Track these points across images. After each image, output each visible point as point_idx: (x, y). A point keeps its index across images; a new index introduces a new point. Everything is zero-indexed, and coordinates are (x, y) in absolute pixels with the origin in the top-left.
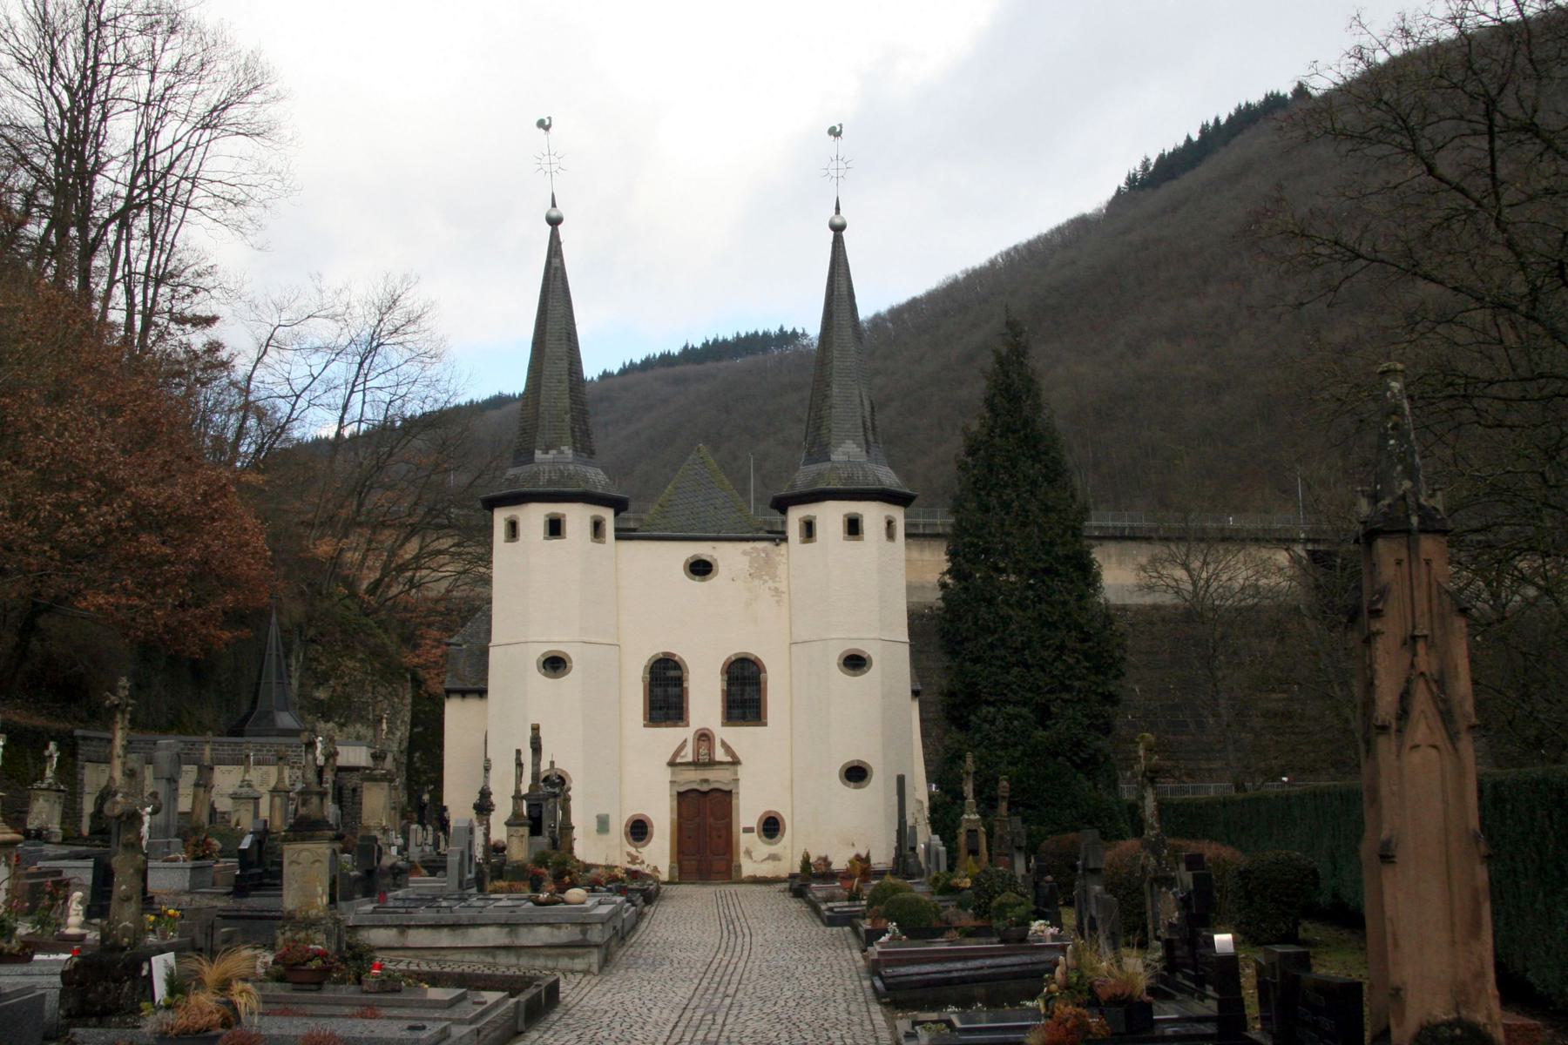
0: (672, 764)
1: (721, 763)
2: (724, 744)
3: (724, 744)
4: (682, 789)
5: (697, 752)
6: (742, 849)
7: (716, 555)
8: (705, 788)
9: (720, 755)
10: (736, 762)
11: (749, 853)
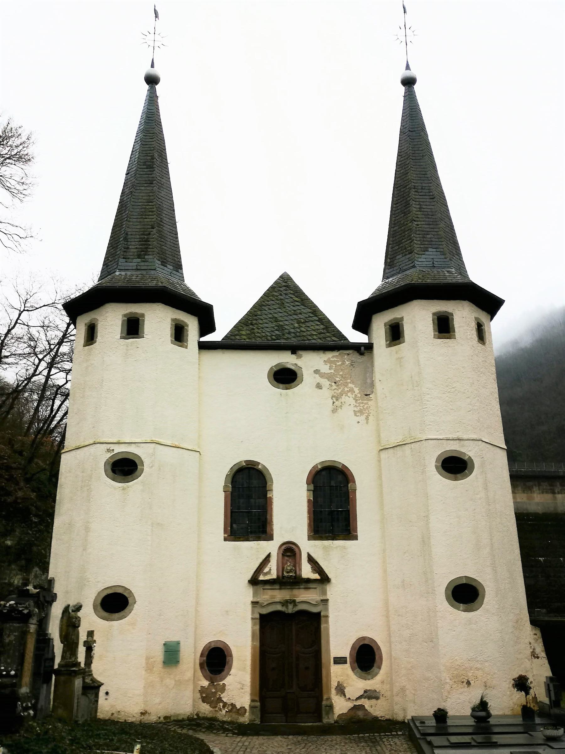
0: (254, 581)
1: (308, 581)
2: (311, 559)
3: (311, 559)
4: (265, 611)
5: (281, 567)
6: (334, 684)
7: (300, 362)
8: (290, 609)
9: (307, 571)
10: (325, 579)
11: (341, 690)
